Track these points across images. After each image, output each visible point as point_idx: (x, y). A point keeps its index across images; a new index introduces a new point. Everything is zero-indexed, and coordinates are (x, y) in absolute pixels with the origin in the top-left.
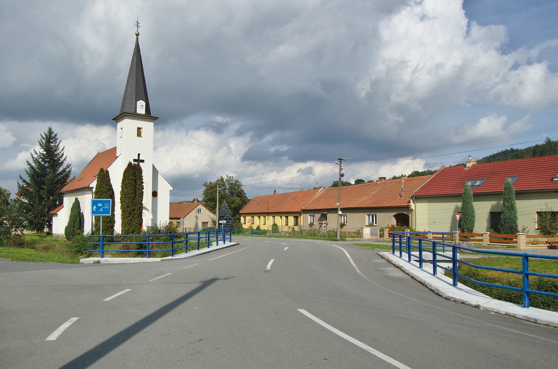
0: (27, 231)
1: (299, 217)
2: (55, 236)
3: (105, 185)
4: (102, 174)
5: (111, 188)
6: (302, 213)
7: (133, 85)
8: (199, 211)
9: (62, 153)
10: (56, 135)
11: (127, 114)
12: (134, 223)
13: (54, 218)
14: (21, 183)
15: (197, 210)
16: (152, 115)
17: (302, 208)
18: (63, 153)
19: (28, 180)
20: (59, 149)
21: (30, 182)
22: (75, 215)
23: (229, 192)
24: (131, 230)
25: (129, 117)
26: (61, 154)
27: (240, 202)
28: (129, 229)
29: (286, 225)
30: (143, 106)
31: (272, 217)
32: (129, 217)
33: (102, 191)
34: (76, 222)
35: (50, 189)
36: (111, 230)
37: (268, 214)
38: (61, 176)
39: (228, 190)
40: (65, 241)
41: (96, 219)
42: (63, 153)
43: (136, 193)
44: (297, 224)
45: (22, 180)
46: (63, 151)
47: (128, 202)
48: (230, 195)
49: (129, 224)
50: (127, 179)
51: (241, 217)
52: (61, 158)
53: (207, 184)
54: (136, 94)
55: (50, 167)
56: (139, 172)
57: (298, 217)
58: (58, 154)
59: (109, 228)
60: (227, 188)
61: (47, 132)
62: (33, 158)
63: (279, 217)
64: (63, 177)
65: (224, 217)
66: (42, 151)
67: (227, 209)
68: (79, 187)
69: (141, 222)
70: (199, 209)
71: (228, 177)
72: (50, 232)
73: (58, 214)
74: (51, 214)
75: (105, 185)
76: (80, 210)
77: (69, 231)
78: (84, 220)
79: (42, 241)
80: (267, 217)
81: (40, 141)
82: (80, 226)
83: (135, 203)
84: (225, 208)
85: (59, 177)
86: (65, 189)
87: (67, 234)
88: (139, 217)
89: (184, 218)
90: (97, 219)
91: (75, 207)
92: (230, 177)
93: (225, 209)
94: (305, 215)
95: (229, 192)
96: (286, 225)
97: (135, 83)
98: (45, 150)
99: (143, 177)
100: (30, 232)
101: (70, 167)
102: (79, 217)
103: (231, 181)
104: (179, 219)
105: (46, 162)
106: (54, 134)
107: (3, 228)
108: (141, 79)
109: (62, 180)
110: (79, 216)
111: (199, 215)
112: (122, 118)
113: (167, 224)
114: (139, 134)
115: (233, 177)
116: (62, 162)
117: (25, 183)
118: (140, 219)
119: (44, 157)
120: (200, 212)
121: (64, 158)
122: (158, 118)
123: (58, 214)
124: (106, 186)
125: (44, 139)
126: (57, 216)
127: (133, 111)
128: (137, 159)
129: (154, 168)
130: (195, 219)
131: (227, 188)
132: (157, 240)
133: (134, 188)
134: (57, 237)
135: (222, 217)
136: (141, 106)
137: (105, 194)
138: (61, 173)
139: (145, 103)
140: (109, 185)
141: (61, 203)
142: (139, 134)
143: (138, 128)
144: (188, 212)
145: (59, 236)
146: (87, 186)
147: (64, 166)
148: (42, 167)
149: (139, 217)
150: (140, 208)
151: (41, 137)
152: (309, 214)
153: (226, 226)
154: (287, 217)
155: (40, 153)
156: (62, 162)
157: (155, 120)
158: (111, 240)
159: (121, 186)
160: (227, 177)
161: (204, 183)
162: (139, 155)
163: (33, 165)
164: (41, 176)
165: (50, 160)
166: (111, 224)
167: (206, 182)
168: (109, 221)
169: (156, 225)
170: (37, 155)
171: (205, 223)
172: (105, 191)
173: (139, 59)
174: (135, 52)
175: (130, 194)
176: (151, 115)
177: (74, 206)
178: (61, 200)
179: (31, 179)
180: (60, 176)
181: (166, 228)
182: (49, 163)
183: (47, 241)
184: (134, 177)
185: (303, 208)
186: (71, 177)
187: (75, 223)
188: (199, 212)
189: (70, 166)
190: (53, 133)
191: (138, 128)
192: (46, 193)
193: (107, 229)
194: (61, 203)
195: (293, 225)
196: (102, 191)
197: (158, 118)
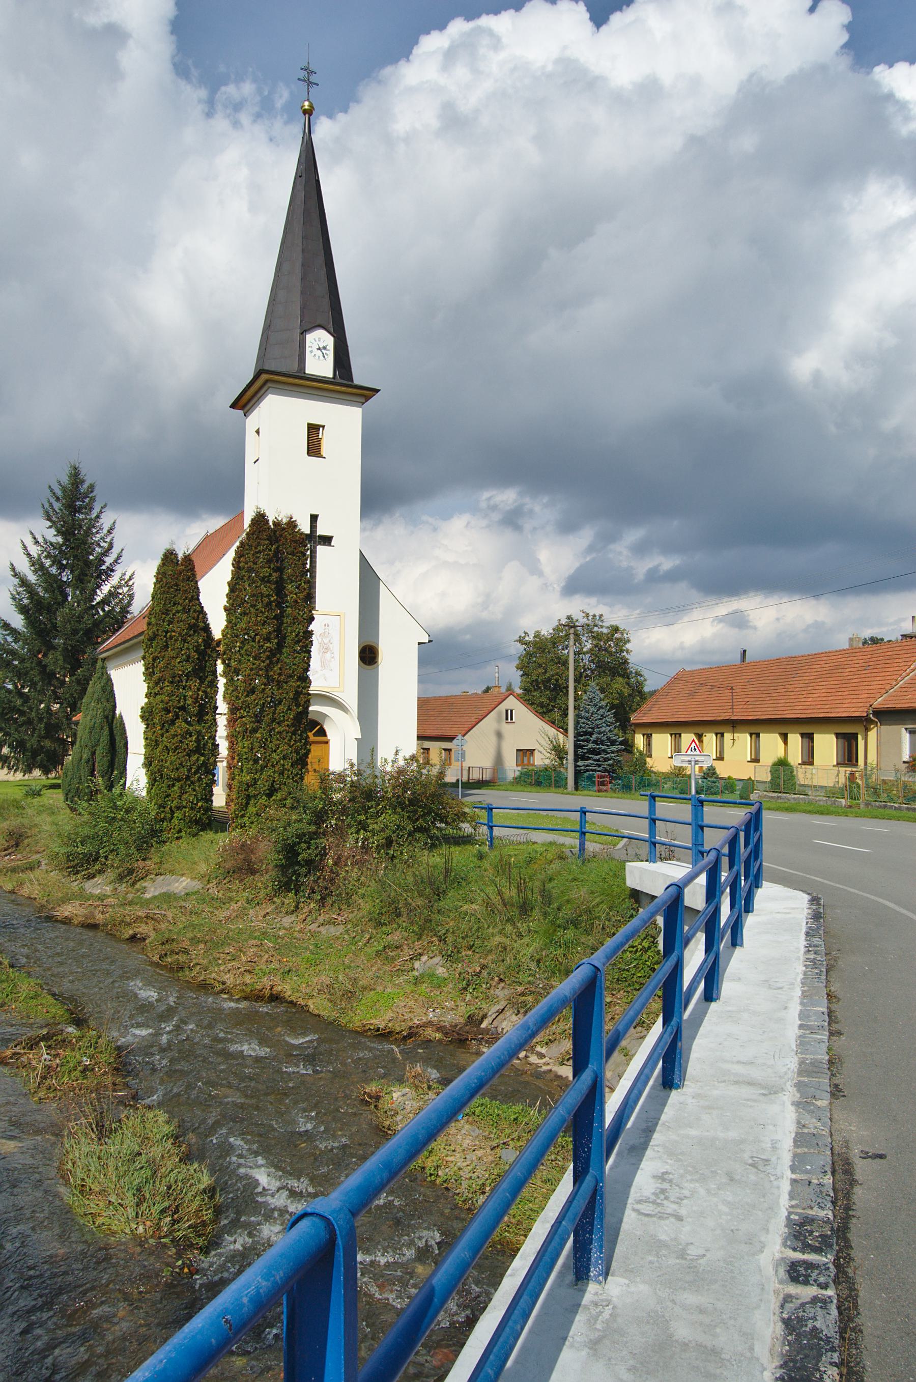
0: (9, 773)
1: (860, 737)
3: (178, 612)
4: (170, 570)
5: (202, 625)
6: (872, 722)
7: (296, 281)
8: (509, 715)
9: (108, 540)
10: (92, 488)
11: (271, 377)
12: (274, 755)
15: (499, 714)
16: (358, 380)
17: (876, 705)
22: (95, 723)
23: (592, 661)
24: (263, 785)
26: (106, 545)
27: (626, 691)
28: (255, 781)
29: (804, 763)
30: (325, 348)
31: (669, 736)
32: (255, 731)
33: (167, 632)
34: (98, 748)
35: (71, 646)
36: (200, 779)
37: (735, 725)
39: (588, 656)
44: (850, 760)
46: (112, 535)
47: (251, 670)
48: (592, 671)
51: (636, 735)
53: (527, 638)
54: (303, 308)
56: (293, 554)
57: (855, 736)
59: (196, 772)
60: (585, 650)
61: (65, 480)
62: (28, 555)
63: (777, 735)
64: (109, 611)
65: (591, 734)
66: (52, 535)
67: (601, 707)
69: (304, 751)
70: (507, 711)
71: (587, 615)
75: (178, 612)
76: (114, 707)
80: (728, 736)
81: (47, 506)
82: (111, 765)
83: (280, 674)
84: (595, 705)
87: (69, 791)
88: (294, 733)
89: (465, 737)
92: (594, 616)
93: (592, 709)
94: (884, 728)
95: (592, 661)
96: (804, 763)
98: (59, 532)
100: (19, 776)
103: (596, 629)
104: (451, 739)
106: (86, 486)
108: (321, 259)
110: (106, 729)
111: (506, 728)
113: (401, 763)
114: (314, 449)
115: (601, 616)
117: (7, 633)
118: (300, 741)
119: (57, 555)
120: (509, 720)
121: (116, 556)
122: (377, 391)
124: (184, 616)
125: (58, 499)
127: (294, 368)
128: (308, 532)
129: (365, 564)
130: (493, 739)
131: (585, 650)
132: (358, 832)
133: (275, 617)
135: (586, 733)
136: (319, 349)
137: (178, 644)
138: (105, 602)
139: (332, 339)
140: (195, 611)
142: (314, 449)
143: (309, 424)
144: (474, 719)
148: (54, 585)
149: (294, 733)
150: (298, 694)
151: (49, 494)
152: (905, 725)
153: (599, 766)
154: (808, 737)
155: (46, 541)
157: (367, 398)
158: (204, 818)
159: (226, 609)
160: (584, 617)
161: (520, 637)
163: (32, 578)
166: (202, 758)
167: (526, 633)
168: (193, 745)
169: (372, 764)
170: (39, 548)
171: (525, 754)
172: (180, 634)
173: (314, 193)
175: (258, 637)
176: (353, 381)
180: (103, 610)
181: (397, 778)
184: (275, 571)
185: (879, 702)
187: (94, 753)
188: (507, 719)
190: (83, 481)
191: (309, 424)
193: (188, 778)
195: (800, 762)
196: (167, 632)
197: (377, 391)
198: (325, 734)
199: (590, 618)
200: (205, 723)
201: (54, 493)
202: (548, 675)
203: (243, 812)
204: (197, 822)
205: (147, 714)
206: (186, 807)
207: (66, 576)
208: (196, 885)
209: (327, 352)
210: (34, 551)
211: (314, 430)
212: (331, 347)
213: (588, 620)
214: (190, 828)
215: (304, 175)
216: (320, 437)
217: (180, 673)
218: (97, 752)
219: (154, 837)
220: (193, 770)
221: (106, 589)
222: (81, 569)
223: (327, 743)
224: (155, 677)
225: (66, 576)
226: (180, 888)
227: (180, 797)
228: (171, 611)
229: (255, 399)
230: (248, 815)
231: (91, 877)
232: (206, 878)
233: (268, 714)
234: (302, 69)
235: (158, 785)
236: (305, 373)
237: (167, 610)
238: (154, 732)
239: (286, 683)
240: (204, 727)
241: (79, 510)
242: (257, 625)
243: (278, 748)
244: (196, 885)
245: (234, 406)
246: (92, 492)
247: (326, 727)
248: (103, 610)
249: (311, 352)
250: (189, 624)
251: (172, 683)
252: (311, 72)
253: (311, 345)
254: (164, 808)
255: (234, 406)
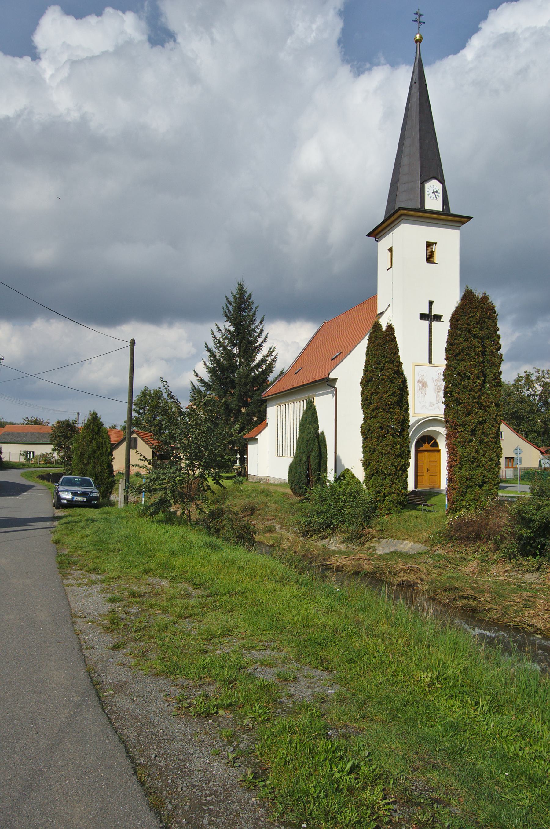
2: (254, 481)
9: (260, 327)
10: (250, 296)
11: (406, 212)
13: (251, 447)
14: (197, 384)
18: (263, 327)
19: (207, 377)
20: (256, 321)
21: (211, 384)
22: (310, 437)
25: (409, 218)
30: (437, 192)
35: (243, 392)
38: (260, 370)
40: (284, 495)
41: (366, 447)
42: (263, 327)
43: (485, 376)
45: (198, 378)
46: (262, 325)
49: (473, 463)
50: (462, 336)
52: (259, 336)
55: (241, 353)
58: (254, 330)
59: (400, 470)
68: (308, 381)
72: (243, 472)
73: (258, 438)
74: (246, 439)
77: (298, 475)
78: (327, 451)
79: (238, 491)
81: (225, 308)
85: (257, 373)
86: (269, 391)
90: (370, 448)
91: (308, 420)
97: (418, 145)
98: (233, 324)
99: (498, 333)
101: (274, 353)
102: (317, 444)
103: (543, 379)
105: (234, 345)
106: (247, 295)
107: (171, 468)
109: (262, 376)
110: (316, 440)
112: (392, 225)
114: (430, 259)
116: (259, 344)
117: (203, 385)
121: (264, 337)
123: (258, 438)
125: (231, 304)
126: (257, 443)
134: (258, 482)
136: (434, 192)
138: (259, 365)
141: (262, 419)
142: (430, 259)
143: (427, 242)
145: (261, 479)
146: (323, 377)
147: (264, 351)
148: (229, 356)
151: (226, 301)
156: (261, 346)
157: (463, 223)
160: (536, 372)
162: (431, 303)
164: (227, 369)
165: (241, 342)
166: (403, 460)
172: (389, 377)
174: (414, 79)
176: (450, 212)
177: (307, 418)
178: (262, 413)
179: (211, 377)
180: (258, 371)
182: (240, 348)
183: (246, 491)
186: (278, 368)
187: (309, 457)
189: (273, 351)
191: (427, 242)
192: (237, 400)
193: (395, 474)
194: (263, 418)
198: (437, 446)
199: (541, 372)
200: (403, 437)
201: (229, 300)
202: (515, 409)
203: (462, 498)
204: (400, 503)
205: (366, 431)
206: (394, 493)
207: (236, 351)
208: (421, 547)
209: (439, 194)
210: (218, 335)
211: (430, 245)
212: (441, 191)
213: (539, 373)
214: (396, 507)
215: (418, 82)
216: (434, 250)
217: (390, 403)
218: (311, 456)
219: (372, 512)
220: (398, 468)
221: (259, 357)
222: (246, 345)
223: (439, 451)
224: (372, 407)
225: (236, 351)
226: (407, 548)
227: (390, 487)
228: (382, 362)
229: (390, 227)
230: (466, 499)
231: (324, 538)
232: (431, 542)
233: (479, 430)
234: (415, 14)
235: (375, 478)
236: (425, 209)
237: (380, 361)
238: (373, 443)
239: (489, 408)
240: (403, 439)
241: (243, 310)
242: (471, 368)
243: (485, 454)
244: (421, 547)
245: (369, 235)
246: (250, 298)
247: (438, 441)
248: (258, 371)
249: (429, 194)
250: (394, 370)
251: (384, 410)
252: (421, 15)
253: (428, 190)
254: (380, 493)
255: (369, 235)
